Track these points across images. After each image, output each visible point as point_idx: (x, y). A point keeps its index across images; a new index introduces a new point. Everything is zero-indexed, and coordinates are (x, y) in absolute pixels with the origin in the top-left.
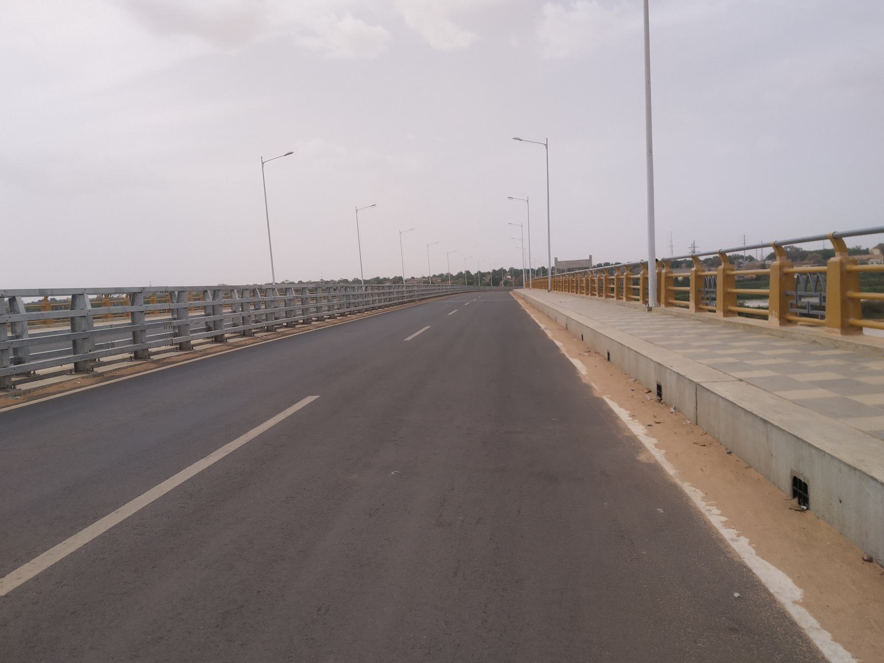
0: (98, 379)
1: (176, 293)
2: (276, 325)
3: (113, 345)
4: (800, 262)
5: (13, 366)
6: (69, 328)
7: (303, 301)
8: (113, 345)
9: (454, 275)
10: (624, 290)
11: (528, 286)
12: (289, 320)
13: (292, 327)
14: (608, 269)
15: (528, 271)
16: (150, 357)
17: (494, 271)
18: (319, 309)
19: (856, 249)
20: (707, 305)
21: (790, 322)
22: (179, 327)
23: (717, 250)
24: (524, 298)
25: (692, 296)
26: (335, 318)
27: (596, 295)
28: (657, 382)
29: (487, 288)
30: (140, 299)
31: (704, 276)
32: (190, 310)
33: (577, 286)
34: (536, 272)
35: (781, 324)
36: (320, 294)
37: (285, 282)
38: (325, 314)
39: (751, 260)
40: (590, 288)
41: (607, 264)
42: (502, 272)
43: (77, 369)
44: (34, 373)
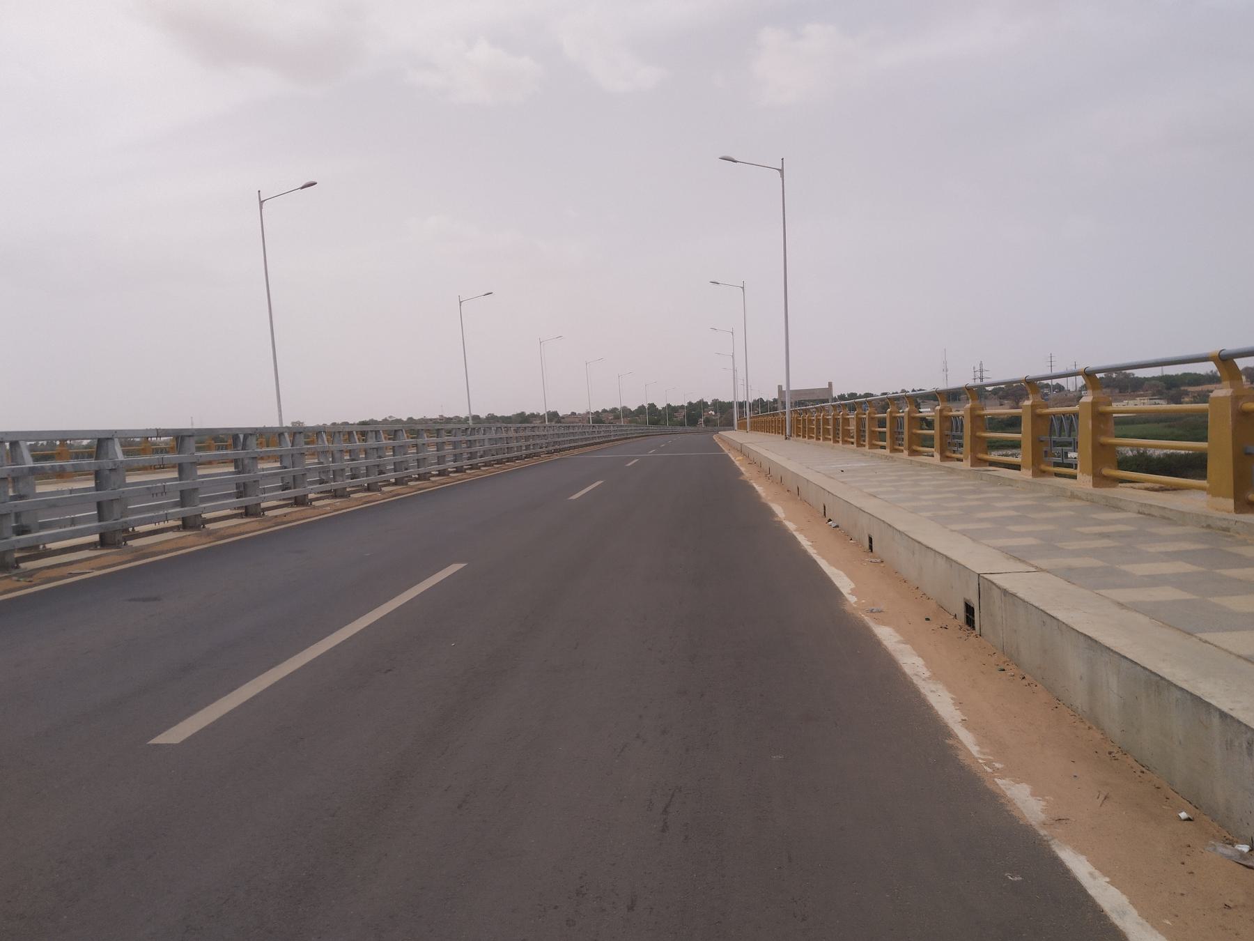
0: (269, 524)
1: (241, 437)
2: (380, 482)
3: (73, 522)
4: (1132, 393)
5: (15, 538)
6: (92, 484)
7: (440, 446)
8: (73, 522)
9: (633, 409)
10: (867, 434)
11: (742, 426)
12: (399, 474)
13: (402, 484)
14: (853, 402)
15: (741, 405)
16: (265, 513)
17: (690, 403)
18: (441, 460)
19: (1210, 374)
20: (954, 452)
21: (1044, 473)
22: (471, 453)
23: (1213, 348)
24: (741, 450)
25: (937, 442)
26: (479, 468)
27: (830, 440)
28: (964, 599)
29: (680, 429)
30: (191, 444)
31: (950, 416)
32: (262, 458)
33: (818, 429)
34: (760, 405)
35: (1095, 485)
36: (425, 439)
37: (388, 418)
38: (450, 465)
39: (1060, 391)
40: (821, 431)
41: (853, 396)
42: (702, 405)
43: (104, 542)
44: (44, 547)
